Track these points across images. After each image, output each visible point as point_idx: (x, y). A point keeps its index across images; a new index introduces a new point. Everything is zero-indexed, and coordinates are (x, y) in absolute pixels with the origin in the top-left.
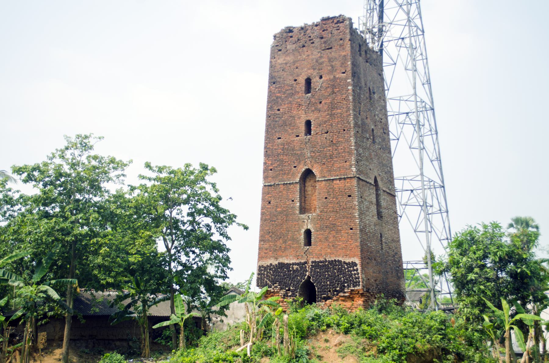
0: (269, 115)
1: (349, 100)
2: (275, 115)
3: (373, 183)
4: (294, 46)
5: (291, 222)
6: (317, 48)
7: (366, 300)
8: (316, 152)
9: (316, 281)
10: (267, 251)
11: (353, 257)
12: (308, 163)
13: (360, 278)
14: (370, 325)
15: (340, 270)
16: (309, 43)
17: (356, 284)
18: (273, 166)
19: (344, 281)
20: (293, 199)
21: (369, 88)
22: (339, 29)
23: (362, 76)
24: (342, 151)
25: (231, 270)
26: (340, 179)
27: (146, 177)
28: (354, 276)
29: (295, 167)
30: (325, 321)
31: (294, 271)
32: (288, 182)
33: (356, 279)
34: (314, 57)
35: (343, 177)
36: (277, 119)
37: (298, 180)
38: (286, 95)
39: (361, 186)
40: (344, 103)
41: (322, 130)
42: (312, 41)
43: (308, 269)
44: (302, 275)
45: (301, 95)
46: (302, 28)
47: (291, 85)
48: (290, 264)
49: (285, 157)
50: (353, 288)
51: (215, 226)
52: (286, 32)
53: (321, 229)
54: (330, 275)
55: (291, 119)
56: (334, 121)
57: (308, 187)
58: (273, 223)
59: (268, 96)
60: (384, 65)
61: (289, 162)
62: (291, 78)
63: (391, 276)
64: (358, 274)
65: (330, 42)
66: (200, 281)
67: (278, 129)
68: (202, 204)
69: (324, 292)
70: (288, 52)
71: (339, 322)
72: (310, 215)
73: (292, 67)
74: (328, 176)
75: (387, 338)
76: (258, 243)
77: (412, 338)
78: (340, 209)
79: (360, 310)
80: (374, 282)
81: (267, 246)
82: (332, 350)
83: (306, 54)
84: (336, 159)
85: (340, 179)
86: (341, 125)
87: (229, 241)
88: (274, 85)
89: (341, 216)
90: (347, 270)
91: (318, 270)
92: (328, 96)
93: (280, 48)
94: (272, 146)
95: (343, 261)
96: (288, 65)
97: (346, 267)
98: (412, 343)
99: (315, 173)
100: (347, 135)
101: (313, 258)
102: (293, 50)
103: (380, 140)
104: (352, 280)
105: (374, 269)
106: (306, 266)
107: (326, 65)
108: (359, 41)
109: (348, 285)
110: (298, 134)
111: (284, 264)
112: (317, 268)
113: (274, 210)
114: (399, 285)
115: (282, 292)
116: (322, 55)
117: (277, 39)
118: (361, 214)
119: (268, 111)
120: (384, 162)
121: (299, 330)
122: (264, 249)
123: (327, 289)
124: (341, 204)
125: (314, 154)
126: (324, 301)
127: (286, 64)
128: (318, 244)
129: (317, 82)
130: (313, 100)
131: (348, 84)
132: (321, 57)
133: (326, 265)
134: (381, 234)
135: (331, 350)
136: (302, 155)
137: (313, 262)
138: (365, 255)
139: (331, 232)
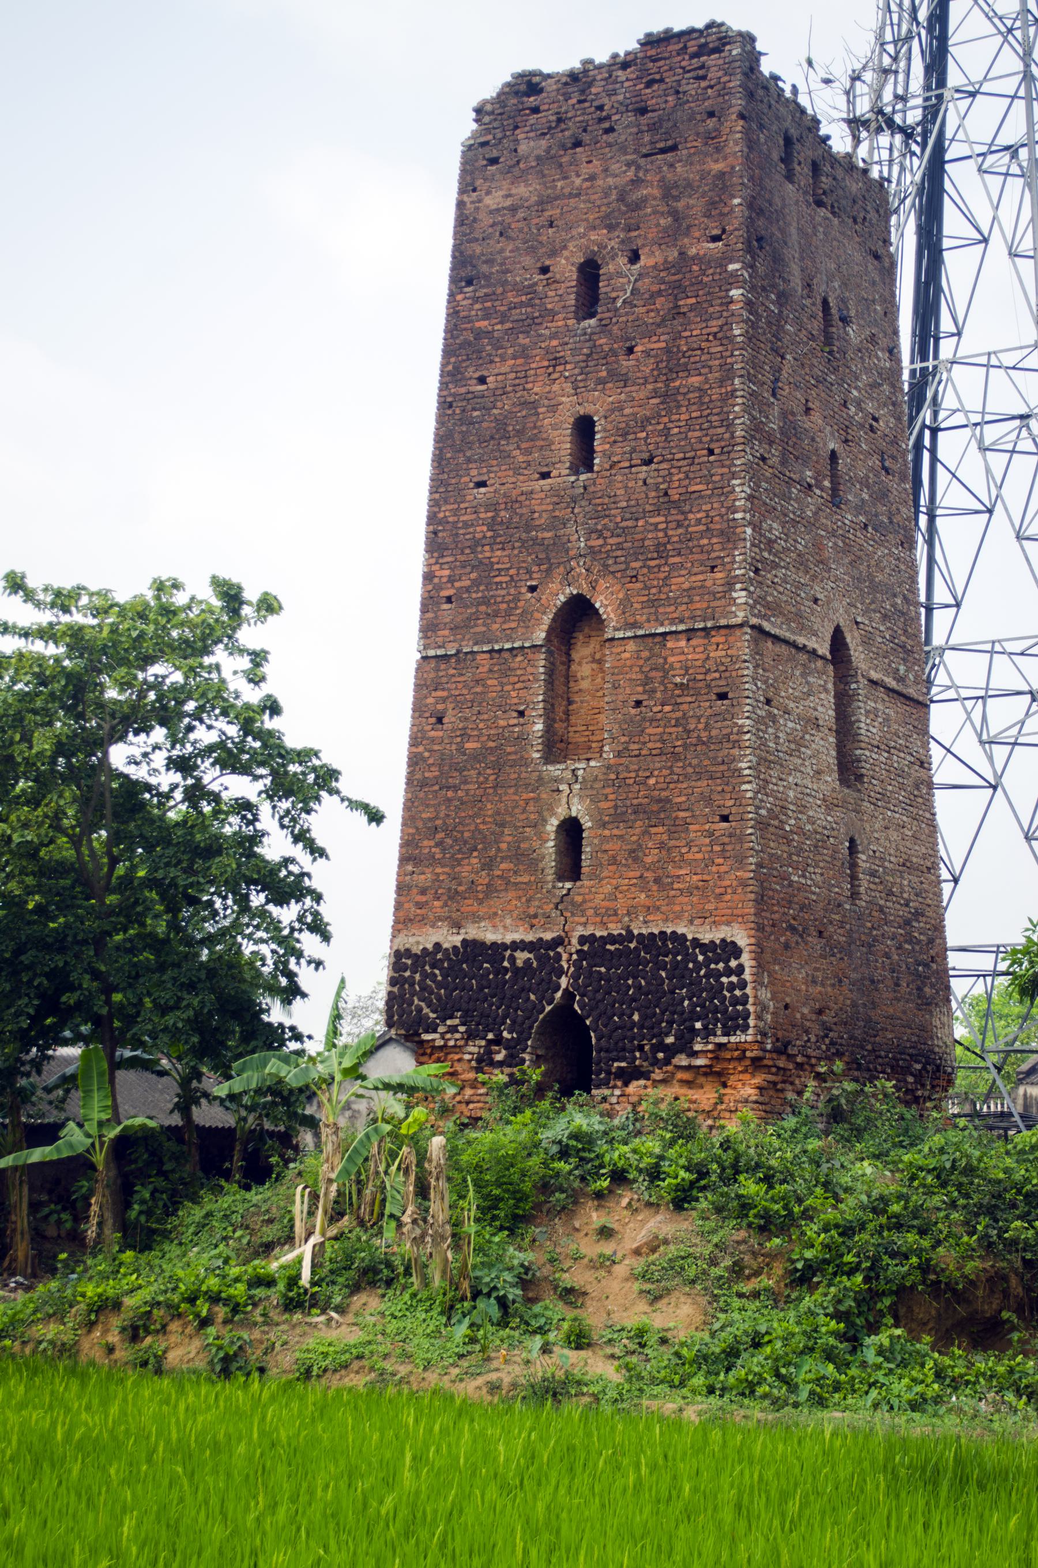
0: (449, 399)
1: (731, 339)
2: (469, 397)
3: (824, 650)
4: (544, 143)
5: (511, 791)
6: (624, 150)
7: (775, 1084)
8: (609, 534)
9: (592, 1009)
10: (423, 899)
11: (728, 923)
12: (581, 574)
13: (751, 1000)
14: (768, 1180)
15: (678, 972)
16: (597, 130)
17: (735, 1023)
18: (457, 584)
19: (693, 1011)
20: (522, 708)
21: (825, 302)
22: (704, 78)
23: (792, 253)
24: (702, 528)
25: (317, 969)
26: (690, 633)
27: (14, 627)
28: (728, 995)
29: (533, 589)
30: (607, 1158)
31: (516, 971)
32: (507, 646)
33: (734, 1005)
34: (610, 181)
35: (701, 625)
36: (476, 414)
37: (540, 635)
38: (509, 325)
39: (768, 660)
40: (713, 350)
41: (633, 450)
42: (606, 125)
43: (566, 966)
44: (544, 986)
45: (560, 323)
46: (573, 77)
47: (530, 286)
48: (504, 946)
49: (499, 553)
50: (724, 1040)
51: (274, 807)
52: (516, 93)
53: (618, 817)
54: (644, 990)
55: (524, 413)
56: (675, 417)
57: (580, 664)
58: (450, 794)
59: (446, 331)
60: (946, 243)
61: (512, 572)
62: (528, 261)
63: (891, 995)
64: (743, 985)
65: (670, 124)
66: (195, 1003)
67: (477, 451)
68: (210, 727)
69: (621, 1053)
70: (522, 165)
71: (657, 1165)
72: (582, 765)
73: (536, 221)
74: (648, 621)
75: (826, 1229)
76: (396, 869)
77: (922, 1232)
78: (685, 746)
79: (746, 1123)
80: (814, 1017)
81: (424, 879)
82: (621, 1270)
83: (586, 170)
84: (677, 560)
85: (690, 633)
86: (698, 434)
87: (321, 861)
88: (471, 289)
89: (690, 770)
90: (702, 973)
91: (603, 970)
92: (659, 326)
93: (495, 154)
94: (455, 512)
95: (690, 937)
96: (521, 214)
97: (701, 958)
98: (919, 1252)
99: (601, 611)
100: (720, 471)
101: (585, 924)
102: (538, 158)
103: (866, 496)
104: (721, 1008)
105: (816, 969)
106: (559, 956)
107: (655, 212)
108: (788, 123)
109: (705, 1027)
110: (545, 469)
111: (483, 944)
112: (598, 960)
113: (454, 747)
114: (925, 1031)
115: (474, 1048)
116: (641, 174)
117: (487, 119)
118: (764, 762)
119: (444, 385)
120: (879, 577)
121: (507, 1191)
122: (415, 891)
123: (631, 1042)
124: (692, 727)
125: (600, 542)
126: (619, 1083)
127: (513, 209)
128: (605, 874)
129: (620, 274)
130: (602, 341)
131: (733, 280)
132: (637, 182)
133: (630, 951)
134: (852, 841)
135: (617, 1268)
136: (560, 545)
137: (582, 940)
138: (776, 916)
139: (653, 830)
